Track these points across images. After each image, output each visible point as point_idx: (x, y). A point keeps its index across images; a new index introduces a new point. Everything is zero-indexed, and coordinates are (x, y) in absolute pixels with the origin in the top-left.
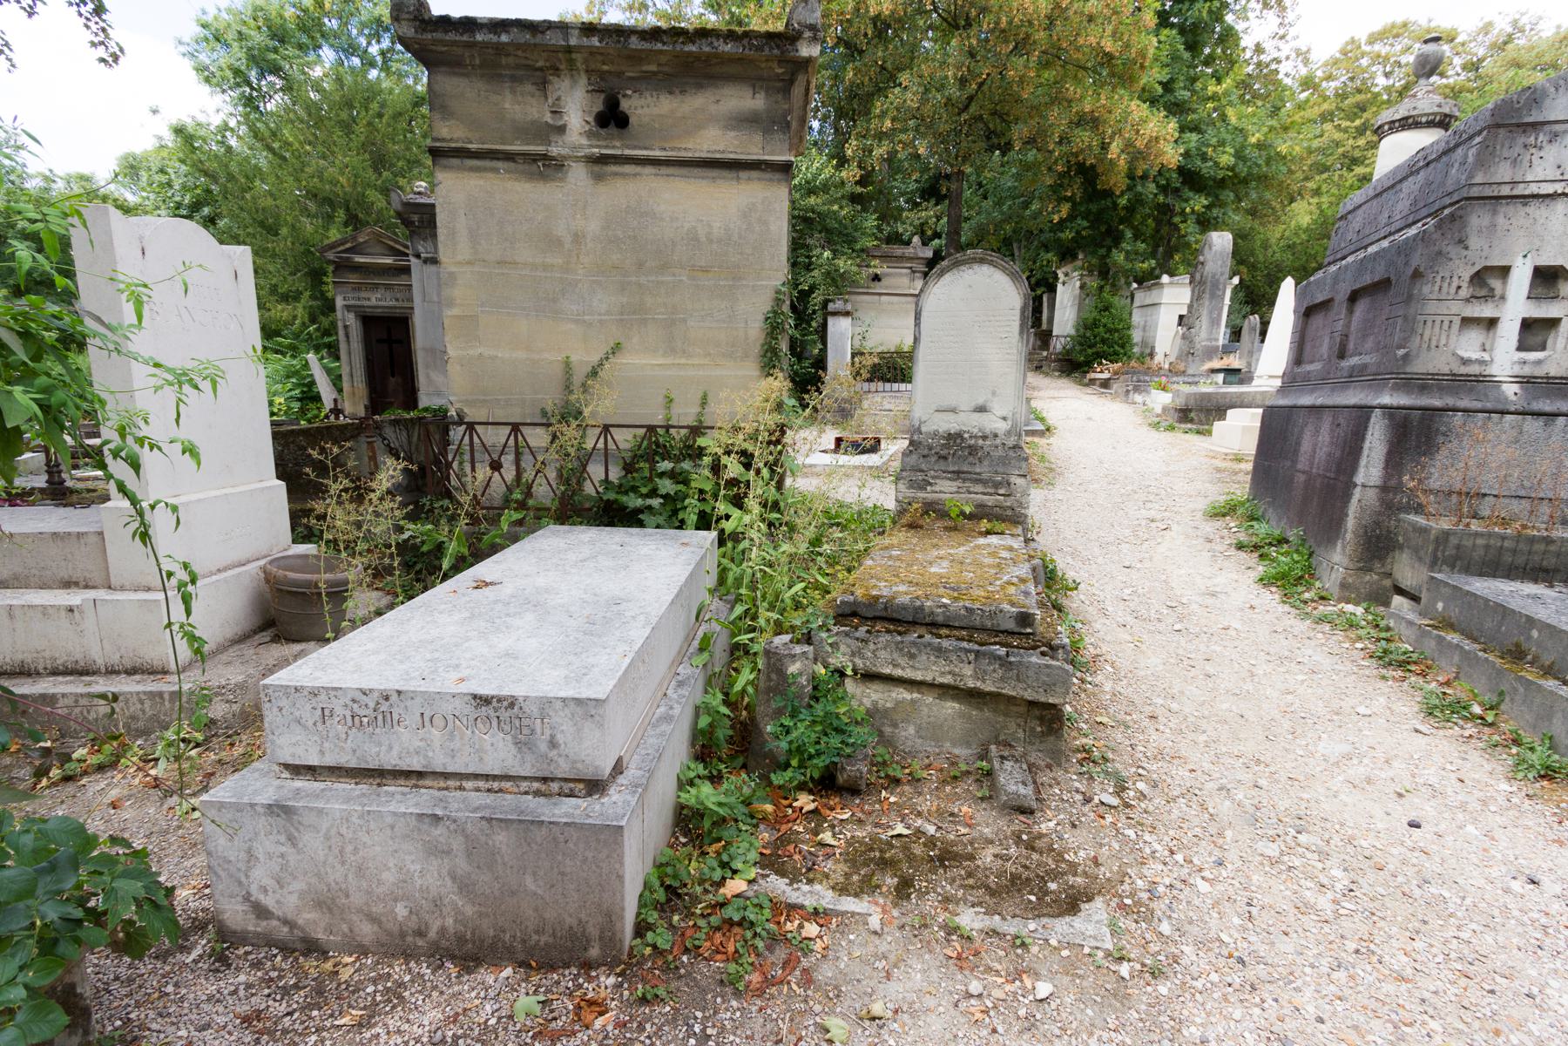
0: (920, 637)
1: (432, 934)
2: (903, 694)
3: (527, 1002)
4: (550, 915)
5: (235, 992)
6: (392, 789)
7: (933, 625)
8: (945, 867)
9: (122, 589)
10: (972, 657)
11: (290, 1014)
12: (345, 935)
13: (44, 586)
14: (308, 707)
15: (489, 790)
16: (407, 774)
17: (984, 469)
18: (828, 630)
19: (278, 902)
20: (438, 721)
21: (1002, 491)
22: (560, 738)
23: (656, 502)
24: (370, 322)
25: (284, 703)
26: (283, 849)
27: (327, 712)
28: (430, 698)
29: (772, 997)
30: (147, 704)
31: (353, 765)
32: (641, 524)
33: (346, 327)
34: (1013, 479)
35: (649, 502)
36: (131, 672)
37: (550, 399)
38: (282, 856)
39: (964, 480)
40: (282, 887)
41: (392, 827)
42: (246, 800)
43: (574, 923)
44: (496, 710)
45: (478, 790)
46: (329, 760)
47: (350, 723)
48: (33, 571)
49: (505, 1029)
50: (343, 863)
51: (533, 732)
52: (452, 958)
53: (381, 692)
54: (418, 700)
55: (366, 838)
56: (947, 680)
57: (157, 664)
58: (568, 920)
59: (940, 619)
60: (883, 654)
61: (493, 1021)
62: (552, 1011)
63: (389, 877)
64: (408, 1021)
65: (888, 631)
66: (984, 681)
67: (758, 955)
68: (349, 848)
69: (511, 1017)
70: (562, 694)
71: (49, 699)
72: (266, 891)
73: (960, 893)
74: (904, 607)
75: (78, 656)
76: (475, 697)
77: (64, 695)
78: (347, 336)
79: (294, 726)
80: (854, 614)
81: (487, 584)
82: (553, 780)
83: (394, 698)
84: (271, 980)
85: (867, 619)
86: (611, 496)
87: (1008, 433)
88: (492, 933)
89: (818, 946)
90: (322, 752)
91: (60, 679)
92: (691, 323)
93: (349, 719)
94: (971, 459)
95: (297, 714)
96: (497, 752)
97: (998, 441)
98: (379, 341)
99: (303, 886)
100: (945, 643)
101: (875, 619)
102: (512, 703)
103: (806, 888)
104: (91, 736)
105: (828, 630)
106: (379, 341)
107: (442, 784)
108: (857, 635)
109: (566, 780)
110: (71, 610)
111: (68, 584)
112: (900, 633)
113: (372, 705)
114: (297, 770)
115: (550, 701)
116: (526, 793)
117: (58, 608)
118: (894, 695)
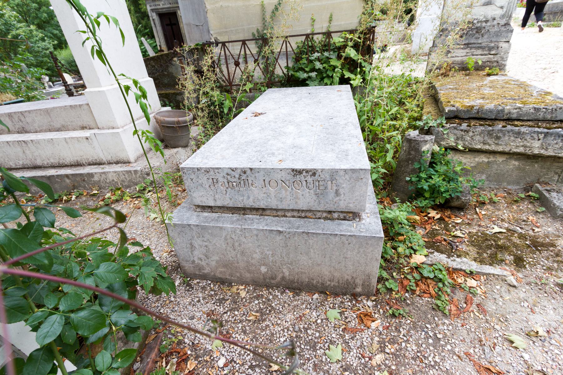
0: (504, 127)
1: (278, 279)
2: (484, 159)
3: (334, 314)
4: (337, 275)
5: (199, 301)
6: (250, 216)
7: (509, 120)
8: (539, 251)
9: (103, 128)
10: (541, 136)
11: (226, 313)
12: (238, 277)
13: (74, 130)
14: (205, 178)
15: (299, 217)
16: (257, 209)
17: (484, 41)
18: (443, 127)
19: (207, 264)
20: (273, 183)
21: (493, 52)
22: (341, 191)
23: (313, 74)
24: (162, 16)
25: (193, 176)
26: (206, 244)
27: (215, 181)
28: (268, 172)
29: (465, 319)
30: (127, 176)
31: (231, 205)
32: (307, 85)
33: (153, 20)
34: (501, 44)
35: (310, 74)
36: (117, 163)
37: (255, 25)
38: (206, 246)
39: (471, 48)
40: (208, 259)
41: (257, 236)
42: (185, 222)
43: (350, 278)
44: (305, 177)
45: (293, 217)
46: (219, 204)
47: (227, 186)
48: (69, 123)
49: (327, 325)
50: (234, 250)
51: (326, 188)
52: (288, 288)
53: (241, 169)
54: (262, 173)
55: (244, 240)
56: (521, 150)
57: (125, 159)
58: (346, 277)
59: (514, 116)
60: (478, 138)
61: (319, 321)
62: (346, 318)
63: (257, 256)
64: (279, 319)
65: (481, 125)
66: (547, 149)
67: (448, 295)
68: (237, 244)
69: (327, 319)
70: (343, 167)
71: (91, 175)
72: (201, 260)
73: (555, 265)
74: (491, 111)
75: (96, 158)
76: (293, 170)
77: (95, 173)
79: (199, 187)
80: (456, 117)
81: (259, 114)
82: (334, 212)
83: (249, 172)
84: (212, 296)
85: (463, 119)
86: (291, 73)
87: (503, 17)
88: (307, 280)
89: (479, 291)
90: (215, 200)
91: (92, 166)
93: (226, 183)
94: (477, 35)
95: (200, 182)
96: (305, 199)
97: (495, 22)
98: (167, 25)
99: (218, 258)
100: (523, 129)
101: (469, 119)
102: (314, 173)
103: (458, 260)
104: (110, 189)
105: (443, 127)
106: (167, 25)
108: (462, 128)
109: (342, 212)
110: (87, 139)
111: (83, 128)
112: (490, 126)
113: (237, 176)
114: (204, 208)
115: (337, 171)
116: (319, 218)
117: (82, 138)
118: (477, 159)
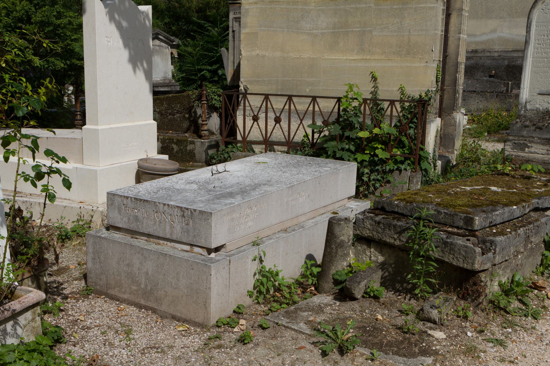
33: (233, 31)
78: (234, 37)
92: (374, 33)
107: (148, 239)
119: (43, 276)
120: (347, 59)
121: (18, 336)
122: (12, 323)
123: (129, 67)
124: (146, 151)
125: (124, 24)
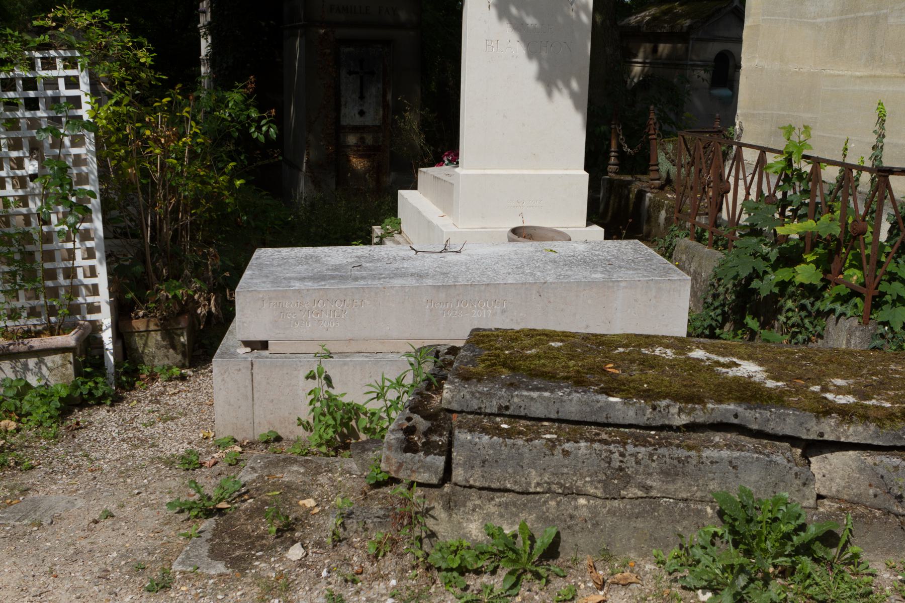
92: (891, 20)
119: (179, 336)
120: (851, 76)
121: (42, 377)
122: (36, 360)
123: (539, 90)
124: (521, 214)
125: (530, 21)
